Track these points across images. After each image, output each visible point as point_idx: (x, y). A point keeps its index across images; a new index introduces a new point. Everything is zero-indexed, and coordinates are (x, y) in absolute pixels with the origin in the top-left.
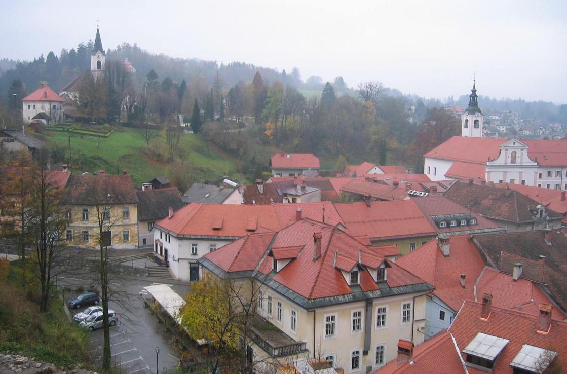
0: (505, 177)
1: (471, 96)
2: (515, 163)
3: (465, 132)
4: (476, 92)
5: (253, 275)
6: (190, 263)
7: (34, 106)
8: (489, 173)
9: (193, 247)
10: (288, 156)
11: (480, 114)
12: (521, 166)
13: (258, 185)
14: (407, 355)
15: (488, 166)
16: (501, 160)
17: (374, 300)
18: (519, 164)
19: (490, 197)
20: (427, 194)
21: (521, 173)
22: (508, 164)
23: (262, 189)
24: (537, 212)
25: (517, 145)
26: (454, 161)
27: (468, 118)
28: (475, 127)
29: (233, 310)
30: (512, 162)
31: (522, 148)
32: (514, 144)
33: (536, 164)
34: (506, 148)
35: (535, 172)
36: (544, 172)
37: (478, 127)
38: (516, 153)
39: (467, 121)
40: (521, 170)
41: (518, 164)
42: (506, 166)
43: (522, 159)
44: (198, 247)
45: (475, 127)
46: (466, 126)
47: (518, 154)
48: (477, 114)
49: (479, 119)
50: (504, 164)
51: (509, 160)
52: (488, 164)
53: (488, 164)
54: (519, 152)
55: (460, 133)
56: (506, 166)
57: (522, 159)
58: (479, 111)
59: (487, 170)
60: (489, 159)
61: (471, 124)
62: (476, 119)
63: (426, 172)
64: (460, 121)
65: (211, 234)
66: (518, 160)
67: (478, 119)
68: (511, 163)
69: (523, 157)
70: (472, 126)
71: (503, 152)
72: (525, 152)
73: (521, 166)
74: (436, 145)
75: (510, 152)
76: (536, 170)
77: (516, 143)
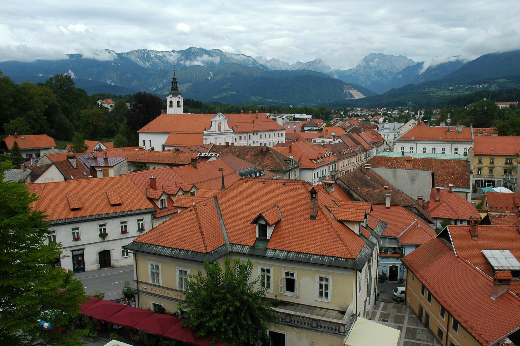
0: (216, 141)
1: (172, 83)
3: (170, 111)
6: (72, 251)
8: (206, 139)
9: (74, 231)
10: (23, 137)
12: (225, 133)
13: (70, 160)
14: (507, 285)
19: (250, 154)
20: (218, 154)
21: (225, 138)
23: (75, 163)
24: (291, 161)
25: (222, 117)
26: (169, 133)
27: (172, 100)
29: (256, 288)
30: (220, 130)
31: (224, 120)
34: (216, 120)
35: (233, 137)
36: (237, 136)
39: (171, 102)
40: (225, 136)
42: (216, 134)
43: (225, 128)
44: (56, 234)
46: (171, 106)
47: (222, 125)
54: (222, 122)
55: (166, 112)
56: (216, 134)
57: (225, 128)
59: (204, 137)
61: (175, 104)
63: (141, 144)
64: (166, 101)
65: (72, 216)
66: (222, 129)
72: (226, 122)
73: (225, 133)
74: (145, 124)
75: (218, 122)
76: (233, 135)
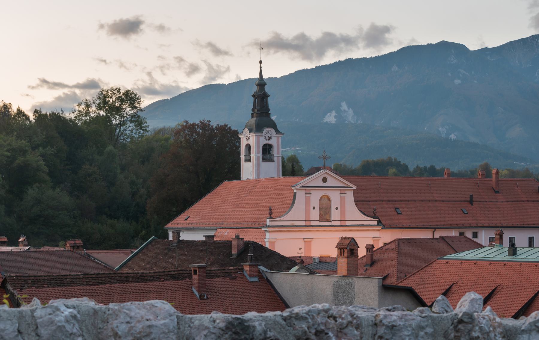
2: (328, 221)
3: (248, 171)
4: (266, 87)
5: (193, 289)
7: (531, 240)
11: (273, 132)
15: (269, 226)
16: (297, 213)
17: (346, 275)
18: (339, 223)
22: (313, 223)
28: (264, 160)
32: (325, 180)
33: (375, 223)
37: (272, 160)
38: (329, 199)
41: (334, 223)
42: (308, 226)
43: (343, 213)
45: (264, 160)
46: (248, 160)
48: (269, 131)
49: (273, 142)
50: (303, 223)
51: (315, 215)
52: (268, 223)
53: (268, 223)
54: (335, 197)
57: (343, 213)
58: (273, 126)
60: (271, 213)
62: (266, 142)
66: (335, 215)
67: (270, 142)
68: (320, 221)
69: (345, 204)
70: (258, 157)
71: (301, 196)
72: (350, 196)
75: (315, 197)
76: (377, 234)
77: (329, 178)
